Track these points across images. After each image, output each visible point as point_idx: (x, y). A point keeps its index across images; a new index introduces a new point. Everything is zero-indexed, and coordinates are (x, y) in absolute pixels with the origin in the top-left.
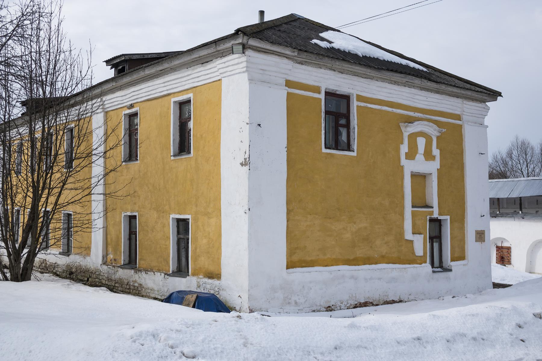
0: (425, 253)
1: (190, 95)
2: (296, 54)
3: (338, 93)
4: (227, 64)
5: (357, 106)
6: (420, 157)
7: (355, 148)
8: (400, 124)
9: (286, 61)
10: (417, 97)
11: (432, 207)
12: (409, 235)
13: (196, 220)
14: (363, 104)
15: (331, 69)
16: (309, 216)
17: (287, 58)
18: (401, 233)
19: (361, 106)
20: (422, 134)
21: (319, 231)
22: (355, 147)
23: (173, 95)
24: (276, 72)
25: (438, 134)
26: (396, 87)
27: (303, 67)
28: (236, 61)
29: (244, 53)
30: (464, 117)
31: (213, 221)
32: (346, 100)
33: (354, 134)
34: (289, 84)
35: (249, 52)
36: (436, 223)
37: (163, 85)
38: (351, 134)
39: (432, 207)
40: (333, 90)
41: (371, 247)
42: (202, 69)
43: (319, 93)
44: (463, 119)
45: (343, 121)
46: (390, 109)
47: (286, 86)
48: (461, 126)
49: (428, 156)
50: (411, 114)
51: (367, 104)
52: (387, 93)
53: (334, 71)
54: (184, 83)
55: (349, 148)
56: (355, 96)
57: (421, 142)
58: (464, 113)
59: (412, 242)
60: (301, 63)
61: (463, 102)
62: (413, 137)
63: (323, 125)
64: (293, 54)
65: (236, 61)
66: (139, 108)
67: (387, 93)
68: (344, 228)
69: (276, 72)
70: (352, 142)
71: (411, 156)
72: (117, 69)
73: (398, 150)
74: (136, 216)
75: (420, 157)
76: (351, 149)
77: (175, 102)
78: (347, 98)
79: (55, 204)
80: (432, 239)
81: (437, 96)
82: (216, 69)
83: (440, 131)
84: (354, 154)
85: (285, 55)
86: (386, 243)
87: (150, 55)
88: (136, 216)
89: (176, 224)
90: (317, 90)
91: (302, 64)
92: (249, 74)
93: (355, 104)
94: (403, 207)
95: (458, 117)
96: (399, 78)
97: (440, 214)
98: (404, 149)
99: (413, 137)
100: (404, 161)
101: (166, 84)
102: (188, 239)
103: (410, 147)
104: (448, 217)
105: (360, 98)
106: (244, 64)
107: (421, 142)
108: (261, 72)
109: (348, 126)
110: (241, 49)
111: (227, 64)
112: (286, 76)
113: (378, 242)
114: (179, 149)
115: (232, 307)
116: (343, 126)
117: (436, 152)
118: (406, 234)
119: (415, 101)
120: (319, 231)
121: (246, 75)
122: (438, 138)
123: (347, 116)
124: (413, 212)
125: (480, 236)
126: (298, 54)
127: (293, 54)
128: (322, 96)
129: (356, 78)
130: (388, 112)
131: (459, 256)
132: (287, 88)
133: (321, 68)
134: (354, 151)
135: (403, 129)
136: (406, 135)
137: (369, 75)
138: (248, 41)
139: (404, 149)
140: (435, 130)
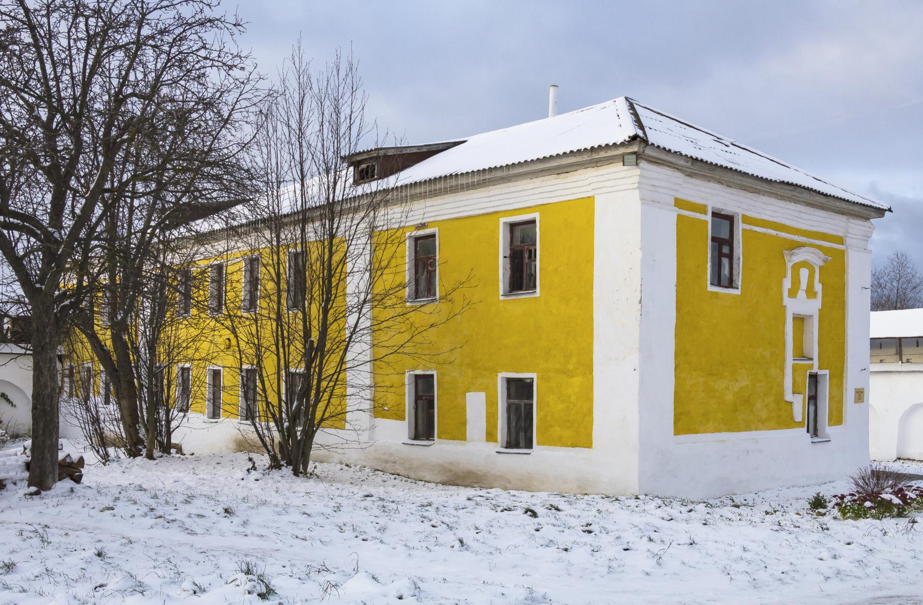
0: (804, 419)
1: (536, 216)
2: (689, 164)
3: (722, 213)
4: (606, 177)
5: (744, 230)
6: (802, 294)
7: (740, 284)
8: (785, 252)
9: (678, 174)
10: (803, 215)
11: (812, 359)
12: (789, 397)
13: (544, 378)
14: (748, 227)
15: (720, 182)
16: (693, 373)
17: (677, 169)
18: (781, 394)
19: (746, 230)
20: (805, 264)
21: (703, 391)
22: (739, 281)
23: (502, 213)
24: (666, 188)
25: (822, 264)
26: (782, 203)
27: (693, 180)
28: (623, 174)
29: (637, 164)
30: (848, 241)
31: (577, 380)
32: (728, 222)
33: (739, 266)
34: (680, 203)
35: (643, 164)
36: (814, 378)
37: (488, 199)
38: (735, 266)
39: (812, 359)
40: (719, 209)
41: (752, 411)
42: (558, 181)
43: (705, 213)
44: (846, 242)
45: (726, 250)
46: (773, 232)
47: (675, 206)
48: (842, 254)
49: (811, 293)
50: (796, 238)
51: (752, 227)
52: (772, 211)
53: (722, 184)
54: (525, 199)
55: (731, 284)
56: (740, 216)
57: (804, 273)
58: (849, 235)
59: (791, 403)
60: (690, 175)
61: (848, 219)
62: (797, 267)
63: (709, 256)
64: (686, 164)
65: (623, 174)
66: (437, 228)
67: (772, 211)
68: (726, 387)
69: (666, 188)
70: (735, 278)
71: (793, 293)
72: (358, 167)
73: (780, 285)
74: (432, 376)
75: (802, 294)
76: (734, 285)
77: (505, 223)
78: (730, 219)
79: (289, 362)
80: (810, 398)
81: (822, 213)
82: (587, 182)
83: (825, 260)
84: (737, 292)
85: (676, 166)
86: (766, 406)
87: (408, 150)
88: (432, 376)
89: (505, 385)
90: (702, 209)
91: (691, 177)
92: (640, 192)
93: (740, 227)
94: (784, 359)
95: (841, 241)
96: (787, 192)
97: (820, 368)
98: (787, 284)
99: (797, 267)
100: (787, 301)
101: (492, 199)
102: (532, 405)
103: (793, 283)
104: (827, 372)
105: (747, 220)
106: (637, 179)
107: (804, 273)
108: (652, 188)
109: (730, 256)
110: (635, 160)
111: (606, 177)
112: (672, 193)
113: (759, 405)
114: (510, 287)
115: (854, 489)
116: (726, 256)
117: (818, 287)
118: (786, 393)
119: (800, 220)
120: (703, 391)
121: (636, 194)
122: (821, 268)
123: (730, 242)
124: (794, 366)
125: (860, 395)
126: (692, 164)
127: (686, 164)
128: (709, 218)
129: (742, 193)
130: (771, 236)
131: (837, 418)
132: (677, 209)
133: (709, 181)
134: (738, 289)
135: (787, 258)
136: (789, 265)
137: (755, 189)
138: (644, 151)
139: (787, 284)
140: (820, 258)
